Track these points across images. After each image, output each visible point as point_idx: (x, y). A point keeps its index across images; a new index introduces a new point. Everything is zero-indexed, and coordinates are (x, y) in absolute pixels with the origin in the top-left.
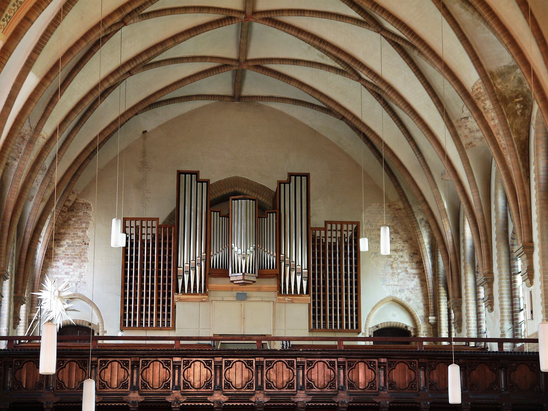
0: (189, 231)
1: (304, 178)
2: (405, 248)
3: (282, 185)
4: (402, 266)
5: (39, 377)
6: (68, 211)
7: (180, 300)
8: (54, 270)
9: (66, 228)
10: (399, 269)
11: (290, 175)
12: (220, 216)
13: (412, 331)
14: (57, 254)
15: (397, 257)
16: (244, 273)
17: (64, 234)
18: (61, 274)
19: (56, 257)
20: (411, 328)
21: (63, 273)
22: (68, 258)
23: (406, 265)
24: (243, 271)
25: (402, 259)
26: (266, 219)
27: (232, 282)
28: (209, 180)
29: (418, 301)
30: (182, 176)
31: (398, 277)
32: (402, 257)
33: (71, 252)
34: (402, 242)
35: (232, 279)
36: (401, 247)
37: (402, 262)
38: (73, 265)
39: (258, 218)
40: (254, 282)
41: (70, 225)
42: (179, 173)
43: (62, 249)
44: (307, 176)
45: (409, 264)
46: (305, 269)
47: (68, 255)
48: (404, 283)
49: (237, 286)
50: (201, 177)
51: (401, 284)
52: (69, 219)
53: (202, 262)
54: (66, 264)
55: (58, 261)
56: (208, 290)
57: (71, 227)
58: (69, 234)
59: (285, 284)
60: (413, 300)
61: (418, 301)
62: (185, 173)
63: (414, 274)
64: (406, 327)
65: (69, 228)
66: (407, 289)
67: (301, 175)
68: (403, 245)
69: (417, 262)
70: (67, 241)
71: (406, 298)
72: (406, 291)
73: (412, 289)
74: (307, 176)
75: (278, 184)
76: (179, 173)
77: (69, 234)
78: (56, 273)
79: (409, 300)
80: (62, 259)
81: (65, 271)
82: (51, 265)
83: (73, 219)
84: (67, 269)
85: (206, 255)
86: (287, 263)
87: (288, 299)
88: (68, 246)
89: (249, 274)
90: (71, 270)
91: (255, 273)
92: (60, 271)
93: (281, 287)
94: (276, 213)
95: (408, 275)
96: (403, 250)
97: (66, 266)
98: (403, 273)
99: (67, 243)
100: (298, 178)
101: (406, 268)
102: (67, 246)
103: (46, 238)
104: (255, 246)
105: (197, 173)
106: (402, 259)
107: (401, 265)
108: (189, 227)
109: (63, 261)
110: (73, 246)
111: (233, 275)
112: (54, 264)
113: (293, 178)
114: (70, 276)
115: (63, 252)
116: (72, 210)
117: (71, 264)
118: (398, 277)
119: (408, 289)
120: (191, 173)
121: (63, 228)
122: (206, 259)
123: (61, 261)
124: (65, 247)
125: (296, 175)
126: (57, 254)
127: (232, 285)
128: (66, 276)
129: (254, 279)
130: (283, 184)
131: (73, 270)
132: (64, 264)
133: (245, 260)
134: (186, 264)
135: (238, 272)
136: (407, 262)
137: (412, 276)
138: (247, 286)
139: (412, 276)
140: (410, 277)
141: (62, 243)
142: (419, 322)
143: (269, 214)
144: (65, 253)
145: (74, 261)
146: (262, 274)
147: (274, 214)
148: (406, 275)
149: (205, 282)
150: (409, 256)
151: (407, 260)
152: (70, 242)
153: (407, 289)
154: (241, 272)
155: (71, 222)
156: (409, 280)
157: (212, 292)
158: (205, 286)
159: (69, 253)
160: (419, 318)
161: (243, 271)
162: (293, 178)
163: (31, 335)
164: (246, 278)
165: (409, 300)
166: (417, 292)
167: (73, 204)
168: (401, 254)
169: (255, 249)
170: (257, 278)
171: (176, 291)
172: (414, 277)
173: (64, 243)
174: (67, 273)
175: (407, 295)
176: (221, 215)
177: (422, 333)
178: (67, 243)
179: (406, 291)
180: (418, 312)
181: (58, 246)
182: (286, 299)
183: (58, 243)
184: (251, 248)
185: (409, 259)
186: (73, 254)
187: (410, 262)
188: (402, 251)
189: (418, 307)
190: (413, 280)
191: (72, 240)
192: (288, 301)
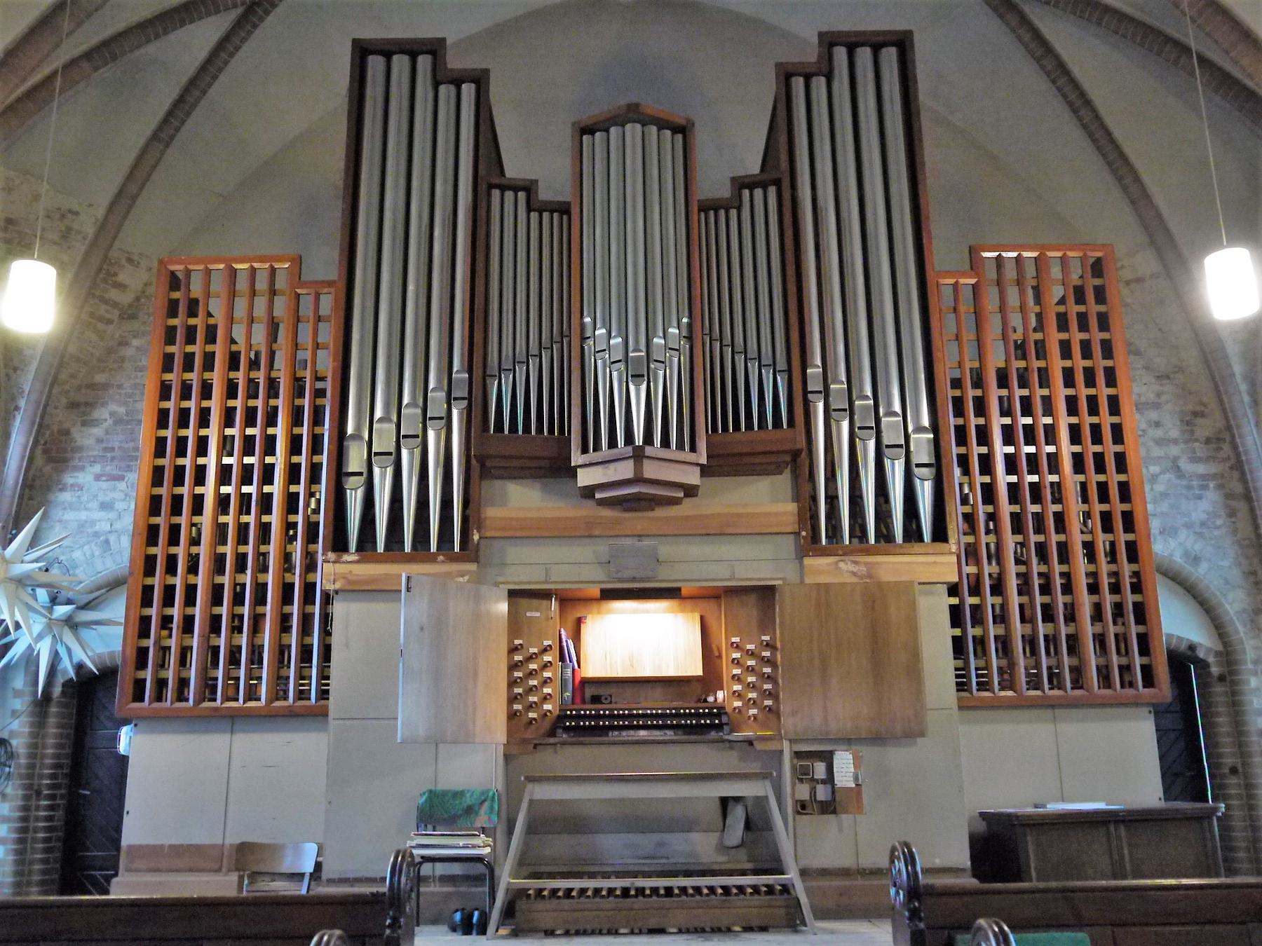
0: (399, 282)
1: (890, 56)
2: (1164, 398)
3: (798, 83)
4: (1162, 453)
5: (1243, 387)
6: (121, 317)
7: (359, 590)
8: (66, 497)
9: (111, 370)
10: (1154, 464)
11: (829, 41)
12: (529, 209)
13: (1211, 659)
14: (81, 449)
15: (1143, 426)
16: (641, 448)
17: (105, 386)
18: (86, 509)
19: (77, 455)
20: (1209, 650)
21: (95, 505)
22: (113, 459)
23: (1174, 451)
24: (639, 439)
25: (1159, 433)
26: (733, 213)
27: (589, 492)
28: (537, 181)
29: (1226, 563)
30: (375, 64)
31: (1152, 489)
32: (1157, 424)
33: (121, 442)
34: (1153, 380)
35: (586, 478)
36: (1151, 396)
37: (1160, 442)
38: (126, 479)
39: (700, 211)
40: (690, 491)
41: (123, 359)
42: (362, 51)
43: (97, 431)
44: (903, 43)
45: (1183, 446)
46: (920, 429)
47: (112, 449)
48: (1172, 507)
49: (606, 512)
50: (455, 62)
51: (1165, 510)
52: (124, 343)
53: (455, 413)
54: (104, 478)
55: (82, 469)
56: (476, 537)
57: (127, 364)
58: (120, 387)
59: (832, 499)
60: (1210, 560)
61: (1226, 563)
62: (387, 50)
63: (1203, 477)
64: (1192, 647)
65: (121, 368)
66: (1183, 526)
67: (877, 43)
68: (1156, 388)
69: (1210, 441)
70: (113, 407)
71: (1186, 554)
72: (1183, 533)
73: (1203, 524)
74: (903, 43)
75: (782, 78)
76: (362, 51)
77: (120, 387)
78: (72, 507)
79: (1196, 560)
80: (94, 462)
81: (102, 498)
82: (59, 482)
83: (135, 342)
84: (108, 493)
85: (470, 378)
86: (839, 402)
87: (851, 567)
88: (117, 422)
89: (665, 454)
90: (121, 496)
91: (693, 449)
92: (85, 498)
93: (815, 517)
94: (777, 183)
95: (1184, 483)
96: (1160, 404)
97: (104, 485)
98: (1167, 476)
99: (112, 414)
100: (864, 54)
101: (1175, 459)
102: (110, 422)
103: (34, 396)
104: (690, 325)
105: (435, 48)
106: (1159, 433)
107: (1157, 452)
108: (400, 266)
109: (97, 468)
110: (128, 422)
111: (592, 456)
112: (69, 479)
113: (841, 54)
114: (112, 515)
115: (100, 441)
116: (133, 317)
117: (121, 478)
118: (1152, 489)
119: (1188, 526)
120: (412, 49)
121: (103, 371)
122: (470, 398)
123: (89, 469)
124: (106, 425)
125: (852, 43)
126: (81, 449)
127: (588, 510)
128: (102, 514)
129: (692, 477)
130: (801, 80)
131: (126, 495)
132: (98, 478)
133: (644, 387)
134: (380, 420)
135: (613, 443)
136: (1175, 442)
137: (1194, 483)
138: (661, 512)
139: (1194, 483)
140: (1189, 488)
141: (97, 414)
142: (1237, 632)
143: (746, 193)
144: (104, 445)
145: (129, 468)
146: (734, 455)
147: (772, 191)
148: (1178, 481)
149: (466, 503)
150: (1182, 421)
151: (1175, 433)
152: (122, 410)
153: (1183, 526)
154: (629, 438)
155: (129, 352)
156: (1187, 498)
157: (496, 543)
158: (465, 520)
159: (116, 444)
160: (1235, 618)
161: (639, 439)
162: (841, 54)
163: (528, 614)
164: (650, 470)
165: (1196, 560)
166: (1216, 533)
167: (138, 299)
168: (1154, 415)
169: (690, 338)
170: (705, 471)
171: (330, 544)
172: (1204, 487)
173: (102, 413)
174: (105, 506)
175: (1189, 544)
176: (533, 206)
177: (1250, 666)
178: (112, 414)
179: (1183, 533)
180: (1230, 596)
181: (84, 424)
182: (842, 565)
183: (84, 414)
184: (673, 331)
185: (1183, 432)
186: (126, 446)
187: (1187, 442)
188: (1156, 406)
189: (1227, 582)
190: (1200, 497)
191: (125, 404)
192: (854, 574)
